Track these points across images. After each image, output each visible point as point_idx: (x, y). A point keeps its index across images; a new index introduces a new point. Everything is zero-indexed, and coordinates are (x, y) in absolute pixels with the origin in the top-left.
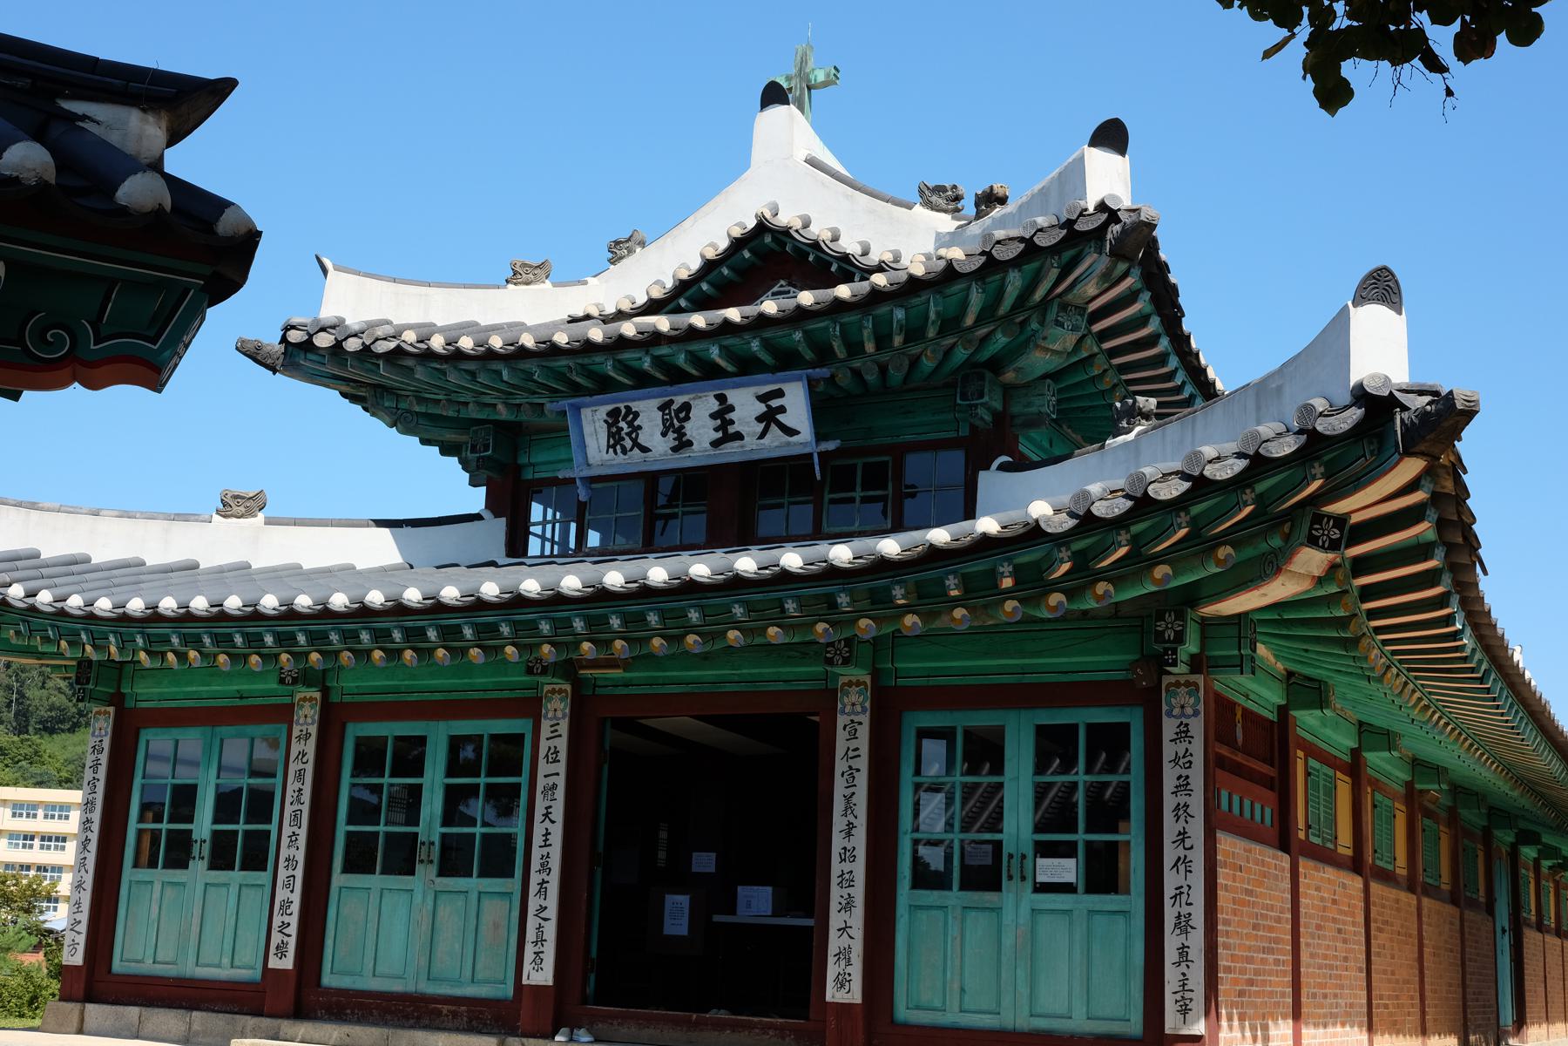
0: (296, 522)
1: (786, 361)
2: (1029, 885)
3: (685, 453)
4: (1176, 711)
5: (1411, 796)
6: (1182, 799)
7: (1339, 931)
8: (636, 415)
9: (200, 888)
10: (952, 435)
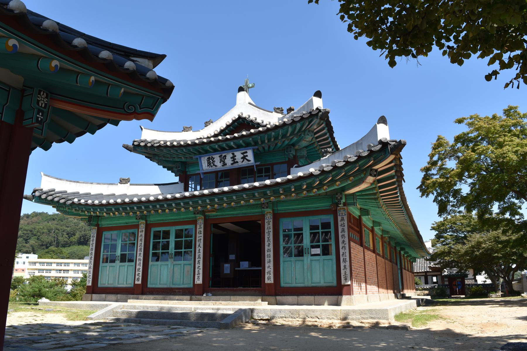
0: (137, 185)
1: (248, 145)
2: (310, 255)
3: (225, 167)
4: (341, 215)
5: (382, 238)
6: (343, 234)
7: (372, 265)
8: (214, 158)
9: (118, 267)
10: (284, 161)
